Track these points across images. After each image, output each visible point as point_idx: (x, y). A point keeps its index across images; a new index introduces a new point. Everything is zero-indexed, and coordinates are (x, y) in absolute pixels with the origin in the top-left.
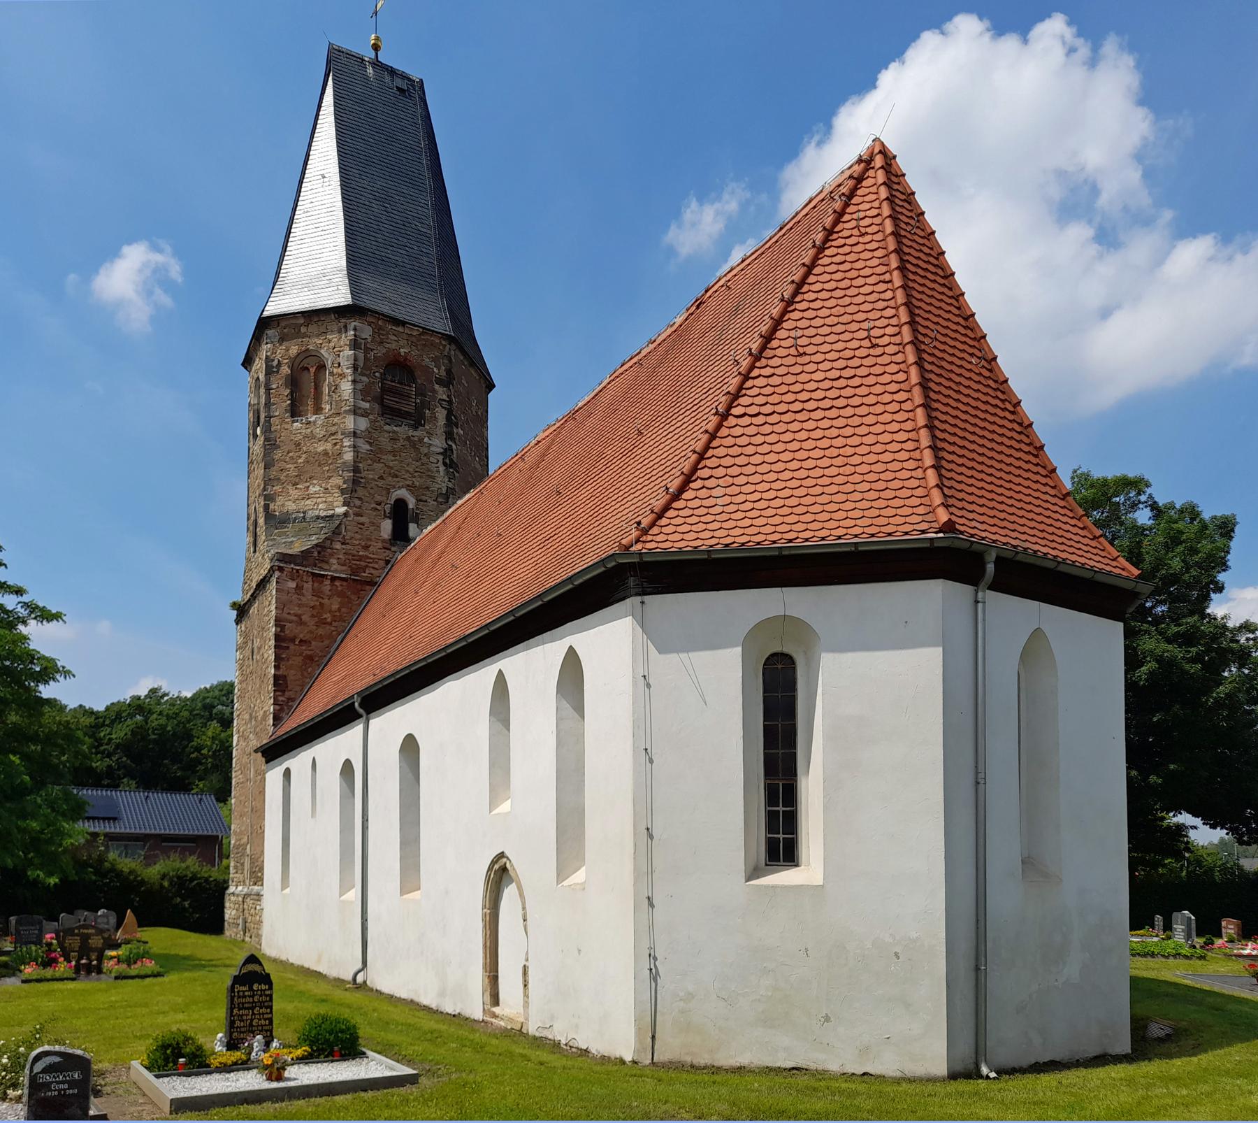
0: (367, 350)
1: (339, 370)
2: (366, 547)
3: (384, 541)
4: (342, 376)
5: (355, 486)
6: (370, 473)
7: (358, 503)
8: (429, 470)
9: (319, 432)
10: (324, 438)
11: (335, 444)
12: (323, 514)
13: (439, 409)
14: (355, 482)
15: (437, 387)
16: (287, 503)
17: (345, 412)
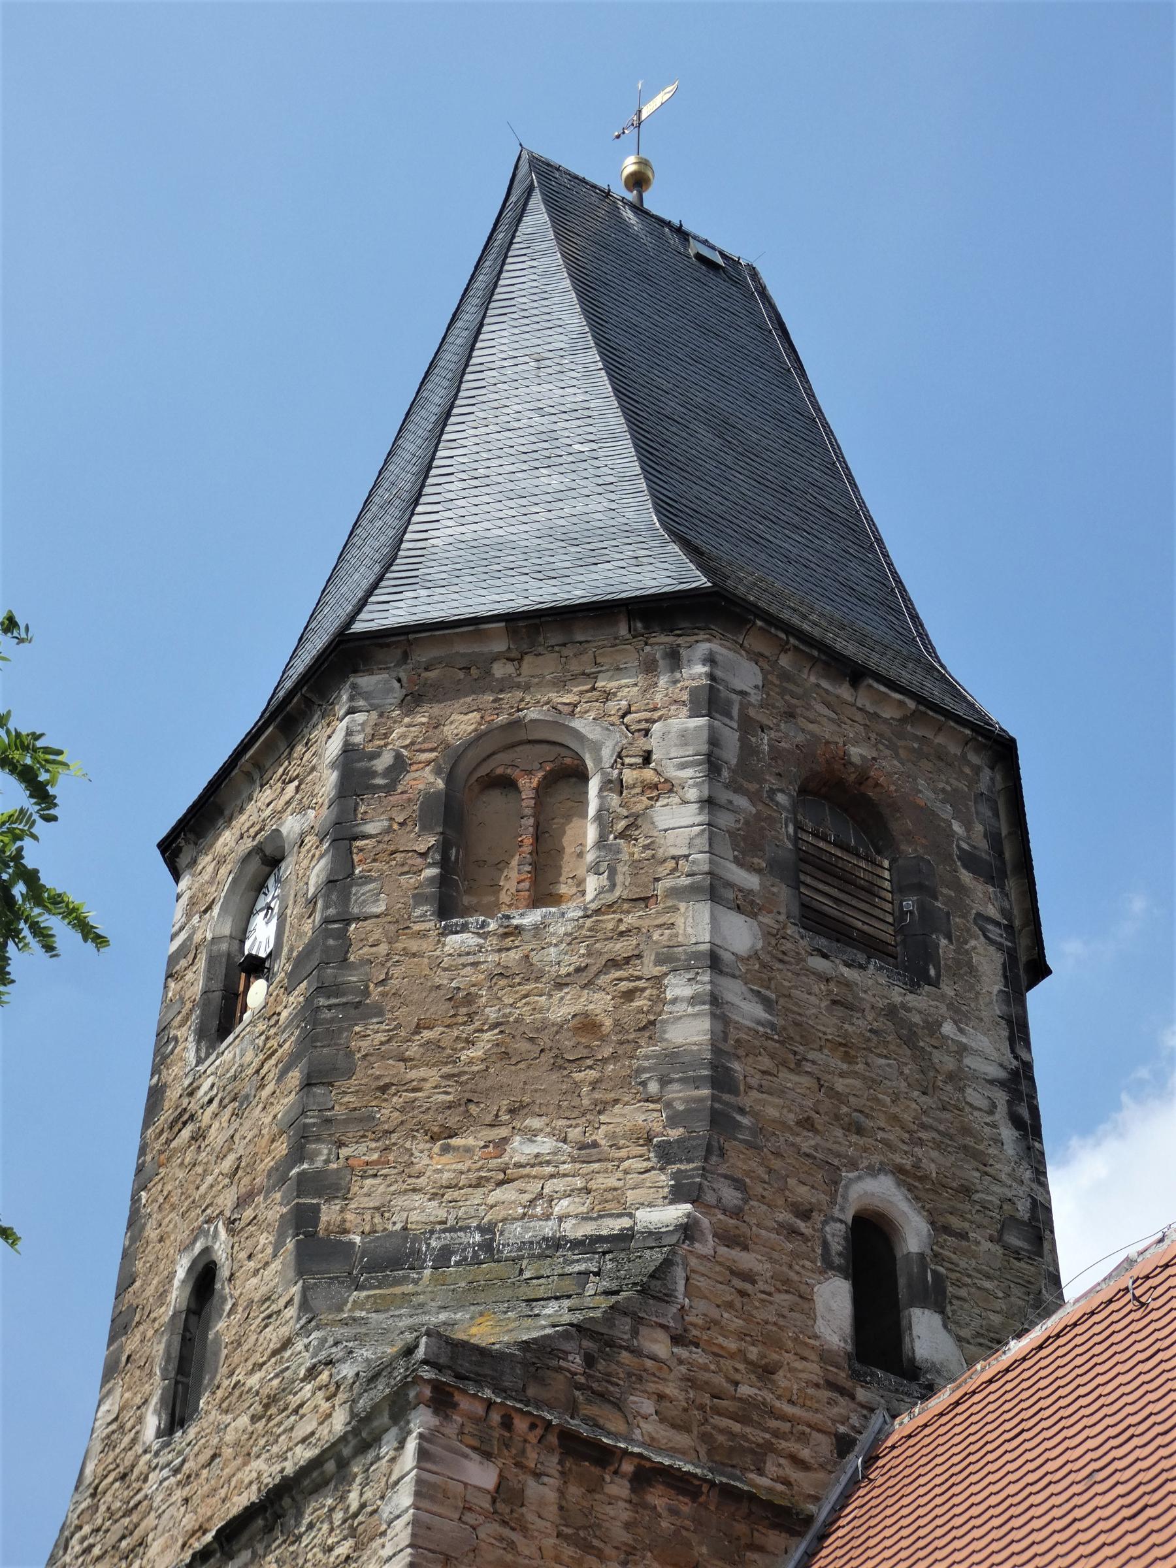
0: (747, 726)
1: (648, 774)
2: (765, 1372)
3: (825, 1356)
4: (662, 788)
5: (714, 1137)
6: (769, 1105)
7: (730, 1196)
8: (966, 1130)
9: (556, 957)
10: (583, 977)
11: (629, 995)
12: (573, 1230)
13: (977, 943)
14: (720, 1121)
15: (966, 876)
16: (405, 1194)
17: (674, 892)
